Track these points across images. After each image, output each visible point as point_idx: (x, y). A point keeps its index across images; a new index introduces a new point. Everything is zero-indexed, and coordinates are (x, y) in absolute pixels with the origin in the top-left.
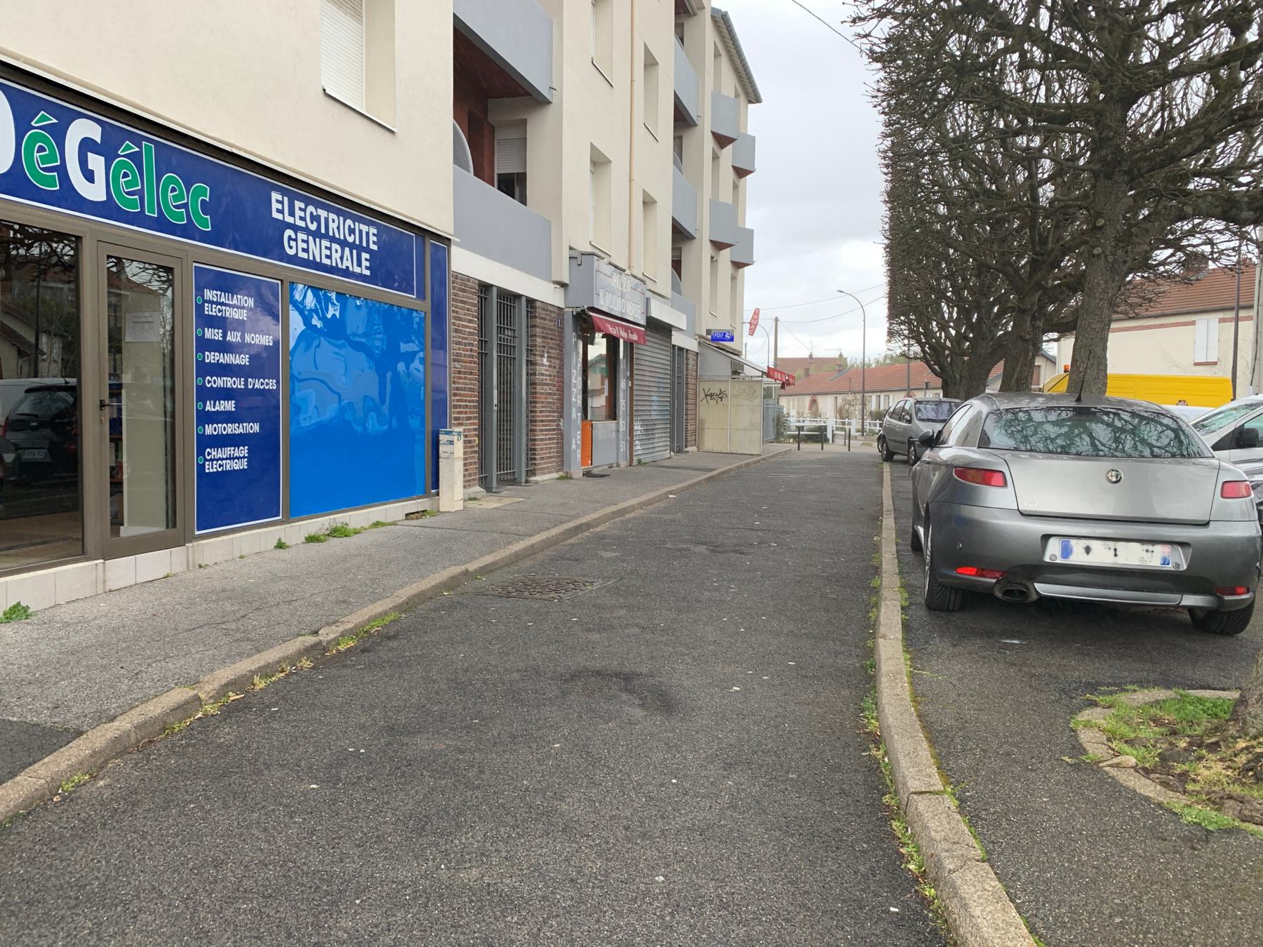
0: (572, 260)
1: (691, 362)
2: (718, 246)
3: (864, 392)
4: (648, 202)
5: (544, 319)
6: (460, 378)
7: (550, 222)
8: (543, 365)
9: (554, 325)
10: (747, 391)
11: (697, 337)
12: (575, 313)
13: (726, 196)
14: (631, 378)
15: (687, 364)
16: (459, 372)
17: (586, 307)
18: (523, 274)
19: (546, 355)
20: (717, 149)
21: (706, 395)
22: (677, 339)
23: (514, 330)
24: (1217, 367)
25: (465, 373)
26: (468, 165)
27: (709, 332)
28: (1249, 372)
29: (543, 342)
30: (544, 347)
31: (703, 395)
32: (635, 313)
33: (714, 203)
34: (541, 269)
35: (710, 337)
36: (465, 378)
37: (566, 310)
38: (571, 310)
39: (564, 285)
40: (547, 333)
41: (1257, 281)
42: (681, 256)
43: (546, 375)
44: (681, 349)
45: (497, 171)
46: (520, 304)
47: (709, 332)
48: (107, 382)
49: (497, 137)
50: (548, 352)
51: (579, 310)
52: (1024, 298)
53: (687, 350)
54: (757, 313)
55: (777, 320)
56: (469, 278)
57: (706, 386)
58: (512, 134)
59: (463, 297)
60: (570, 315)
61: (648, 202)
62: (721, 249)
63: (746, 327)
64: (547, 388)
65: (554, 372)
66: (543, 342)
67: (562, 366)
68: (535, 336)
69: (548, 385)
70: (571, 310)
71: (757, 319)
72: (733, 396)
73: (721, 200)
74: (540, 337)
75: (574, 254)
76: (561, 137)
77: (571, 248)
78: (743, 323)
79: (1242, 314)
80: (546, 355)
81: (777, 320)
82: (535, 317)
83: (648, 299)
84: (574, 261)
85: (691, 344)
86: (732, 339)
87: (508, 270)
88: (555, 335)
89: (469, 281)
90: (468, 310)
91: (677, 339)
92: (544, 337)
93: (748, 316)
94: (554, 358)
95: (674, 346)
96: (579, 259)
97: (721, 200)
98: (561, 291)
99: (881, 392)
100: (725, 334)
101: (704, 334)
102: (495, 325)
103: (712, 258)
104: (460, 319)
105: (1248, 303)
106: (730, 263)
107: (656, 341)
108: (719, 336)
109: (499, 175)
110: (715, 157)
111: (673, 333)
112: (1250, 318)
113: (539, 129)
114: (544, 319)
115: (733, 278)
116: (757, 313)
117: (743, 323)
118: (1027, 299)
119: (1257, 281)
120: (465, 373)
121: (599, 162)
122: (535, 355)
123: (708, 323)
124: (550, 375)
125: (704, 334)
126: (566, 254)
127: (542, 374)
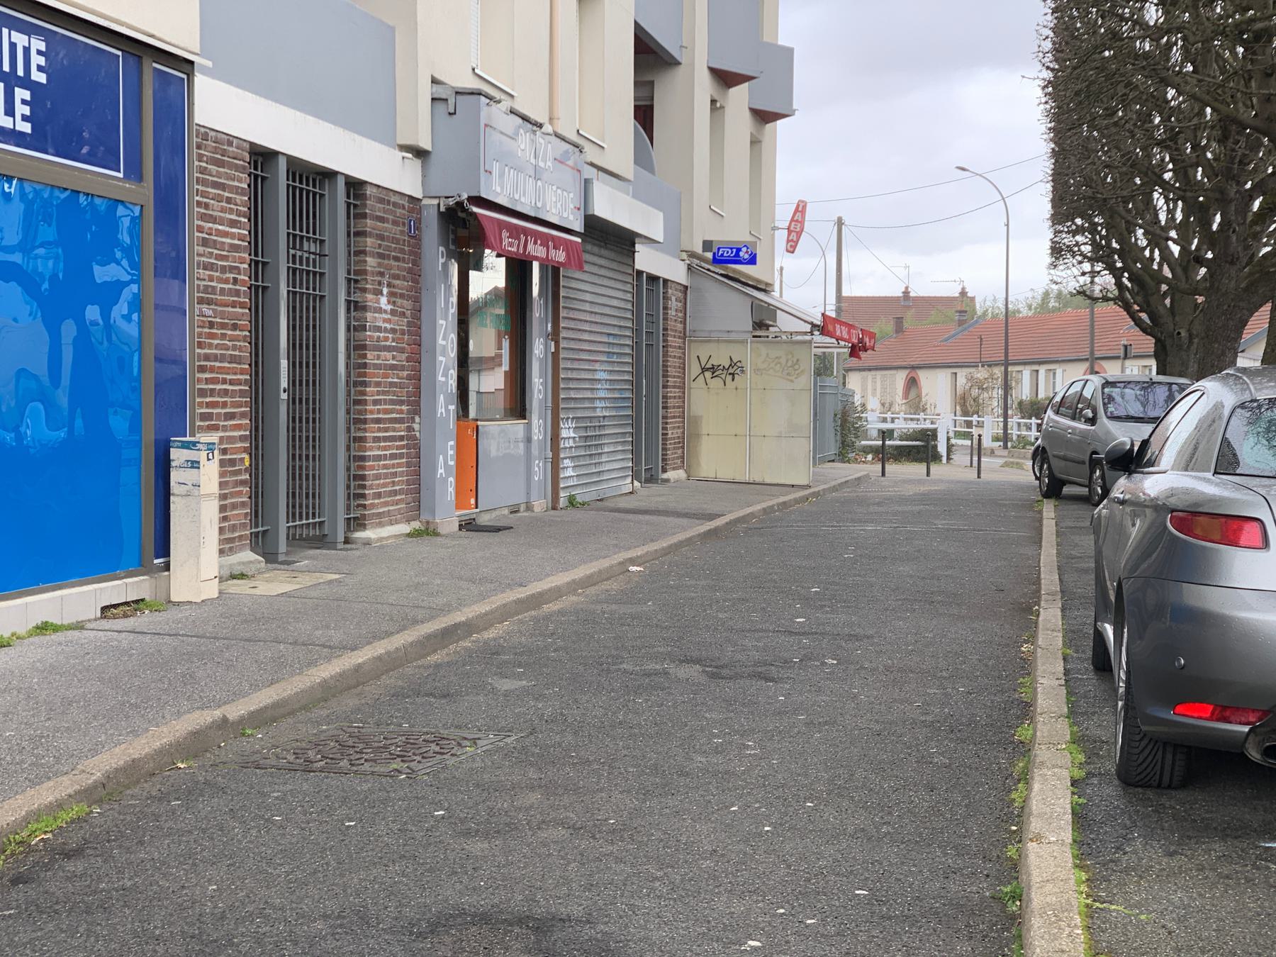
0: (437, 103)
1: (674, 304)
2: (725, 79)
5: (382, 219)
8: (380, 310)
9: (402, 232)
10: (783, 361)
11: (684, 256)
12: (442, 209)
14: (555, 335)
15: (665, 308)
16: (211, 325)
17: (465, 196)
19: (385, 291)
21: (704, 370)
22: (645, 260)
23: (322, 242)
25: (223, 326)
27: (707, 245)
30: (382, 274)
36: (223, 336)
37: (425, 202)
38: (435, 202)
39: (420, 153)
42: (652, 99)
43: (386, 330)
44: (653, 279)
47: (707, 245)
51: (451, 202)
53: (666, 281)
54: (801, 209)
55: (840, 223)
56: (230, 139)
57: (704, 351)
60: (434, 213)
63: (781, 236)
64: (388, 355)
65: (403, 324)
66: (380, 265)
67: (417, 311)
70: (435, 202)
71: (802, 222)
77: (434, 81)
78: (774, 229)
80: (385, 291)
81: (840, 223)
82: (364, 216)
85: (672, 269)
86: (752, 261)
88: (402, 251)
89: (230, 144)
90: (229, 200)
91: (645, 260)
92: (381, 256)
93: (783, 215)
94: (402, 296)
99: (1040, 363)
100: (739, 250)
103: (713, 102)
104: (214, 220)
106: (747, 114)
108: (728, 254)
111: (638, 247)
115: (755, 142)
116: (801, 209)
117: (774, 229)
120: (223, 326)
122: (364, 290)
124: (393, 331)
127: (379, 329)
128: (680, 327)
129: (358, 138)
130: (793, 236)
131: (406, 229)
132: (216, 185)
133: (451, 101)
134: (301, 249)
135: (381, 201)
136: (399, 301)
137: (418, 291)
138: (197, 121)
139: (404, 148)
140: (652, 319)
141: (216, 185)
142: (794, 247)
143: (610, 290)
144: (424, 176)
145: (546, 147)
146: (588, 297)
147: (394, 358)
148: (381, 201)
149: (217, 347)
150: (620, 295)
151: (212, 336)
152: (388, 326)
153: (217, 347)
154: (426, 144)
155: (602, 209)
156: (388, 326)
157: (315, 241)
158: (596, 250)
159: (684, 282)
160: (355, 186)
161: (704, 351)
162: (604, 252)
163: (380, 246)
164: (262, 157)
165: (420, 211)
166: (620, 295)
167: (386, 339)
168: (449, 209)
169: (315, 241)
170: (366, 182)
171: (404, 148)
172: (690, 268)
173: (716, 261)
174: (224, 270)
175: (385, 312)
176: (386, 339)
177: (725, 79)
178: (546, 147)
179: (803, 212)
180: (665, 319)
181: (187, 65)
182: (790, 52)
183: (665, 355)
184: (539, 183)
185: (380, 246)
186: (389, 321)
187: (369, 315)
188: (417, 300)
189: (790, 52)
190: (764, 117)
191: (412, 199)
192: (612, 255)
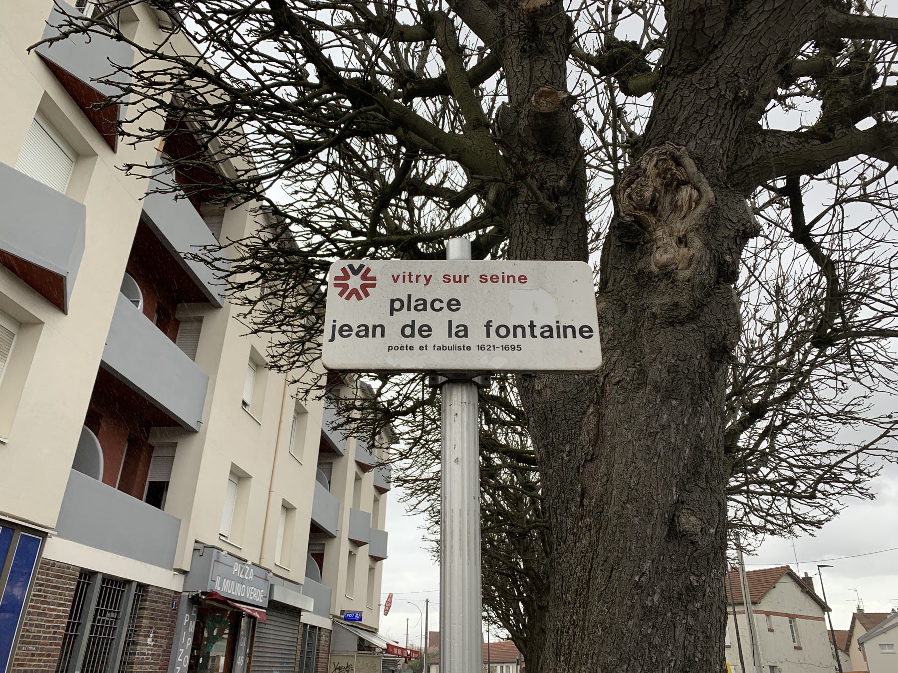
0: (196, 551)
1: (323, 638)
2: (356, 544)
3: (489, 663)
4: (287, 508)
5: (156, 602)
6: (34, 660)
7: (180, 521)
8: (147, 645)
9: (167, 608)
10: (369, 665)
11: (331, 617)
12: (190, 597)
13: (366, 505)
14: (250, 655)
15: (319, 640)
16: (33, 655)
17: (200, 591)
18: (138, 563)
19: (151, 635)
20: (360, 473)
21: (336, 669)
22: (305, 618)
23: (118, 613)
24: (731, 649)
25: (40, 655)
26: (98, 472)
27: (342, 612)
28: (751, 658)
29: (150, 623)
30: (151, 628)
31: (333, 669)
32: (258, 596)
33: (355, 512)
34: (166, 561)
35: (343, 616)
36: (40, 660)
37: (183, 594)
38: (187, 594)
39: (185, 573)
40: (157, 615)
41: (742, 585)
42: (324, 550)
43: (148, 654)
44: (313, 627)
45: (148, 480)
46: (130, 589)
47: (342, 612)
48: (301, 594)
49: (154, 454)
50: (154, 633)
51: (194, 594)
52: (541, 597)
53: (320, 628)
54: (390, 597)
55: (427, 601)
56: (68, 566)
57: (336, 660)
58: (166, 452)
59: (57, 583)
60: (186, 598)
61: (287, 508)
62: (359, 546)
63: (382, 608)
64: (147, 666)
65: (160, 651)
66: (150, 623)
67: (169, 646)
68: (142, 617)
69: (151, 663)
70: (187, 594)
71: (391, 603)
72: (357, 669)
73: (361, 509)
74: (147, 618)
75: (198, 546)
76: (201, 457)
77: (197, 542)
78: (380, 605)
79: (737, 609)
80: (151, 635)
81: (427, 601)
82: (146, 600)
83: (272, 586)
84: (197, 552)
85: (325, 623)
86: (360, 619)
87: (131, 562)
88: (165, 616)
89: (68, 568)
90: (60, 594)
91: (305, 618)
92: (151, 619)
93: (383, 601)
94: (161, 638)
95: (306, 625)
96: (201, 549)
97: (361, 509)
98: (182, 578)
99: (503, 663)
100: (355, 615)
101: (338, 614)
102: (93, 606)
103: (350, 552)
104: (49, 603)
105: (740, 601)
106: (368, 557)
107: (282, 620)
108: (351, 616)
109: (151, 483)
110: (358, 479)
111: (302, 613)
112: (743, 612)
113: (185, 452)
114: (156, 602)
115: (371, 569)
116: (390, 597)
117: (380, 605)
118: (543, 598)
119: (742, 585)
120: (40, 655)
121: (239, 476)
122: (138, 635)
123: (341, 604)
124: (153, 655)
125: (338, 614)
126: (191, 545)
127: (144, 654)
128: (327, 649)
129: (148, 565)
130: (387, 608)
131: (170, 606)
132: (54, 587)
133: (201, 551)
134: (104, 616)
135: (157, 593)
136: (159, 640)
137: (172, 635)
138: (43, 556)
139: (176, 570)
140: (311, 645)
141: (54, 587)
142: (387, 613)
143: (747, 627)
144: (185, 582)
145: (250, 570)
146: (272, 636)
147: (151, 668)
148: (157, 593)
149: (34, 666)
150: (291, 635)
151: (34, 660)
152: (150, 652)
153: (34, 666)
154: (187, 569)
155: (277, 597)
156: (150, 652)
157: (114, 612)
158: (279, 615)
159: (330, 629)
160: (142, 587)
161: (336, 660)
162: (282, 616)
163: (152, 614)
164: (87, 575)
165: (180, 598)
166: (291, 635)
167: (148, 659)
168: (193, 597)
169: (114, 612)
170: (148, 585)
171: (176, 570)
172: (333, 622)
173: (345, 619)
174: (49, 627)
175: (150, 645)
176: (148, 659)
177: (356, 544)
178: (250, 570)
179: (391, 598)
180: (319, 645)
181: (45, 535)
182: (387, 533)
183: (317, 662)
184: (244, 586)
185: (152, 614)
186: (151, 650)
187: (139, 647)
188: (171, 639)
189: (387, 533)
190: (376, 559)
191: (176, 592)
192: (286, 617)
